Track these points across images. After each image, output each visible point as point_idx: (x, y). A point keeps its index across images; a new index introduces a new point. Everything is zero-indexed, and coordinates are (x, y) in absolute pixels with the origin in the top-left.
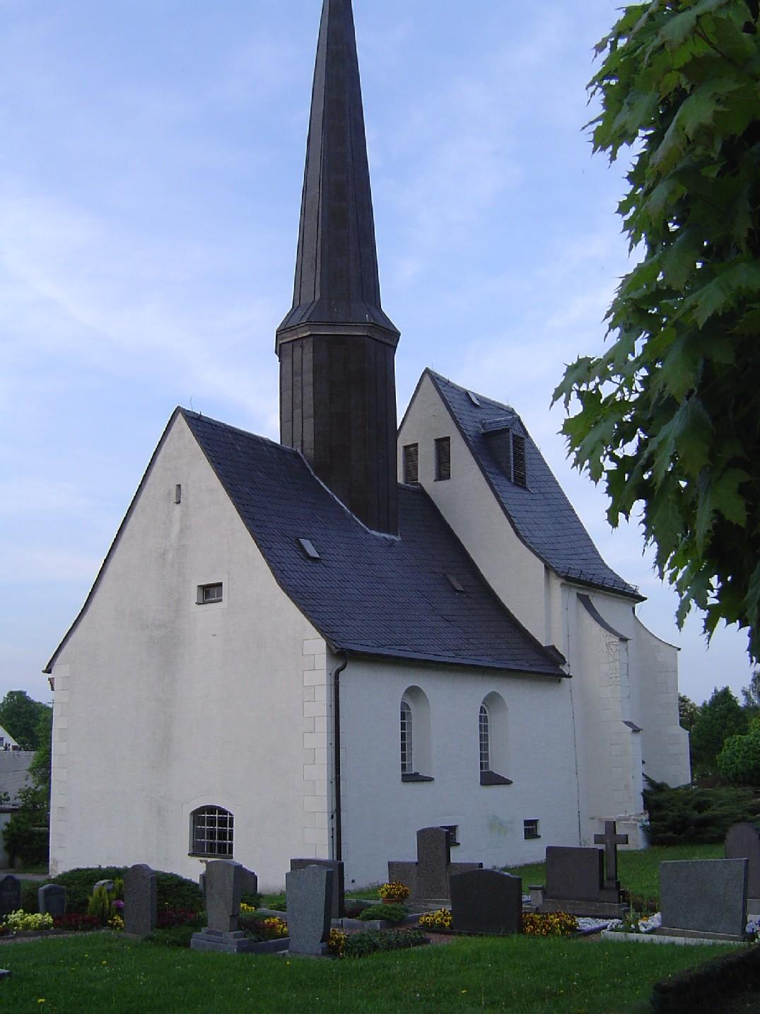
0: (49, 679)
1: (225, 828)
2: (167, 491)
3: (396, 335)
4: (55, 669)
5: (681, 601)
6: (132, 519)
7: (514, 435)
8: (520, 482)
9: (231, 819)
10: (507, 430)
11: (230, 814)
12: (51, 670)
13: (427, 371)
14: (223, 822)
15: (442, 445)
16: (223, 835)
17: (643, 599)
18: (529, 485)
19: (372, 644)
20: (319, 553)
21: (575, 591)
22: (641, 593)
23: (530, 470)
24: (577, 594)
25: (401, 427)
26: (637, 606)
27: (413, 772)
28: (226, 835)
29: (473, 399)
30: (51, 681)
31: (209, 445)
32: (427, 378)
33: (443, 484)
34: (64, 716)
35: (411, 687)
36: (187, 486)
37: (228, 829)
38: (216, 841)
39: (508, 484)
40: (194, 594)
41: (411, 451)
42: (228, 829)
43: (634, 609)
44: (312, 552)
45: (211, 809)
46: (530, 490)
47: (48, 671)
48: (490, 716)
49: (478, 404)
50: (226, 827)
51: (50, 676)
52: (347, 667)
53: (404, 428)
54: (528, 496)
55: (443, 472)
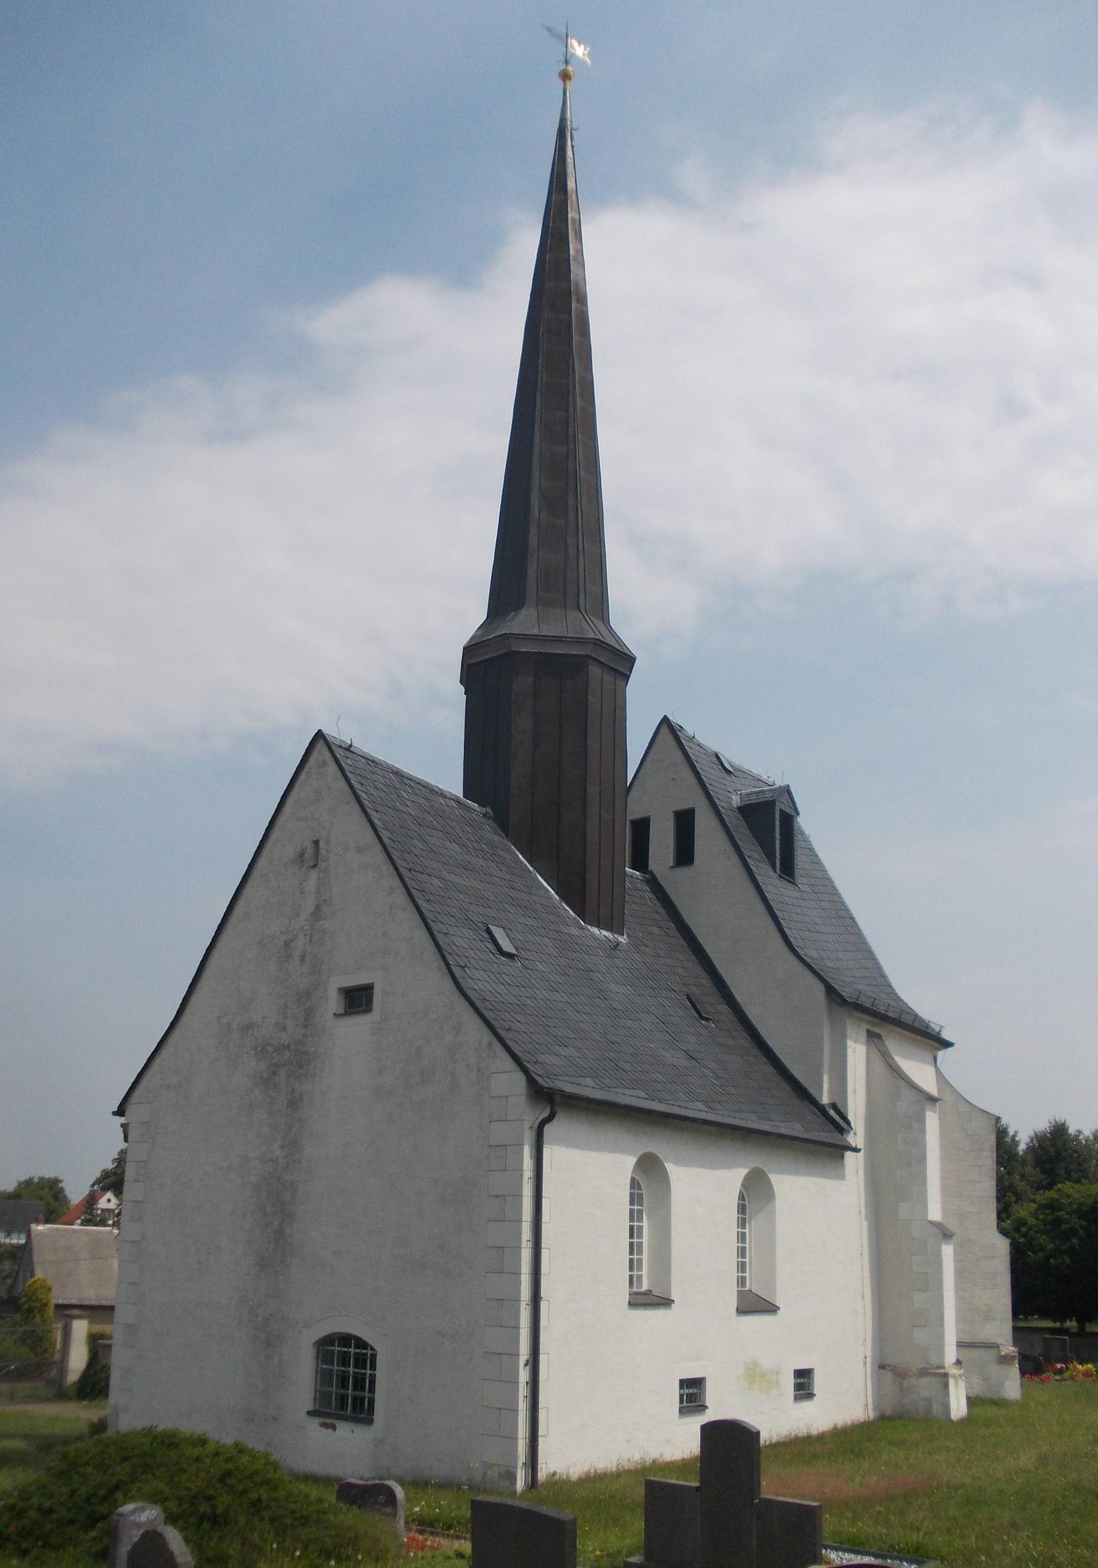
0: (122, 1125)
1: (363, 1371)
2: (299, 850)
3: (630, 660)
4: (130, 1109)
5: (91, 1191)
6: (248, 890)
7: (781, 810)
8: (788, 870)
9: (374, 1357)
10: (772, 803)
11: (372, 1349)
12: (124, 1112)
13: (665, 720)
14: (360, 1362)
15: (685, 821)
16: (359, 1383)
17: (947, 1044)
18: (799, 880)
19: (594, 1085)
20: (516, 949)
21: (865, 1026)
22: (946, 1035)
23: (801, 861)
24: (868, 1031)
25: (632, 783)
26: (941, 1054)
27: (643, 1290)
28: (365, 1384)
29: (725, 764)
30: (124, 1126)
31: (362, 784)
32: (665, 730)
33: (683, 872)
34: (139, 1181)
35: (647, 1153)
36: (328, 842)
37: (369, 1372)
38: (351, 1369)
39: (772, 874)
40: (334, 1002)
41: (641, 828)
42: (369, 1372)
43: (935, 1059)
44: (507, 946)
45: (346, 1339)
46: (799, 885)
47: (120, 1112)
48: (748, 1204)
49: (732, 770)
50: (365, 1369)
51: (122, 1120)
52: (555, 1121)
53: (637, 783)
54: (797, 894)
55: (684, 855)
